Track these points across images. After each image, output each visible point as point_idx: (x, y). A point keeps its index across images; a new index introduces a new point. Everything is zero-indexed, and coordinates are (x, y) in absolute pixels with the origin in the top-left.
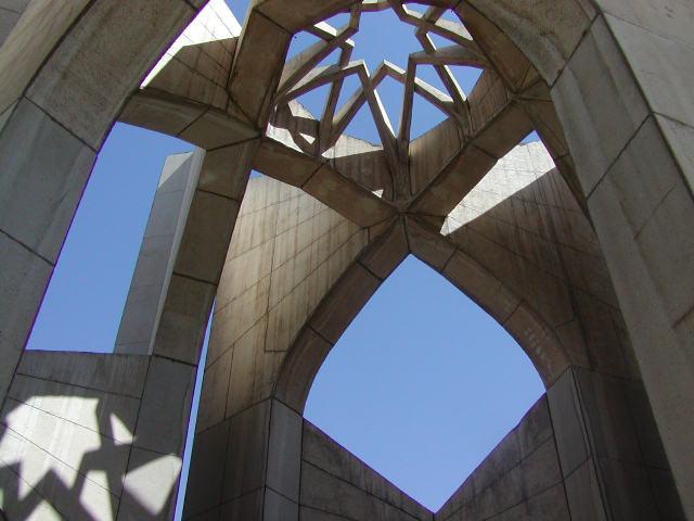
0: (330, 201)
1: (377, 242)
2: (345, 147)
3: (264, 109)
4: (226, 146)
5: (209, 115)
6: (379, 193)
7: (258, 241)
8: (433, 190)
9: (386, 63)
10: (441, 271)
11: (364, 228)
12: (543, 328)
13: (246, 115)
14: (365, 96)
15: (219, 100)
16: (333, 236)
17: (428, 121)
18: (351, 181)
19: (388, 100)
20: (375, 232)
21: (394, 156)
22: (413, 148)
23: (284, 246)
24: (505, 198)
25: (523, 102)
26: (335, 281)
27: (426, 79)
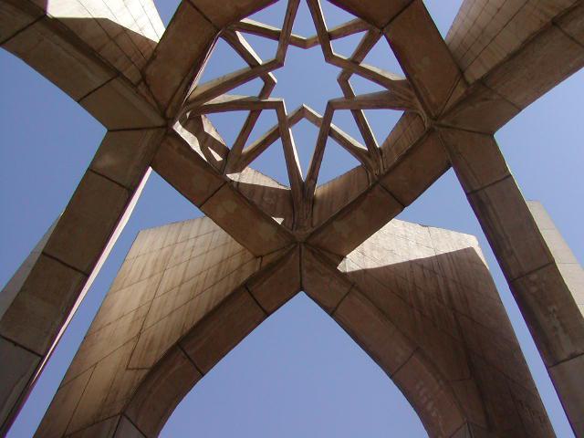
0: (225, 224)
1: (269, 270)
2: (248, 176)
3: (177, 97)
4: (128, 130)
5: (116, 83)
6: (279, 221)
7: (147, 274)
8: (336, 224)
10: (332, 312)
11: (257, 257)
12: (438, 381)
13: (157, 102)
14: (280, 133)
15: (135, 77)
16: (223, 267)
17: (337, 165)
18: (252, 203)
19: (302, 139)
20: (267, 260)
21: (300, 194)
22: (318, 191)
23: (172, 276)
24: (405, 260)
25: (441, 130)
26: (216, 304)
27: (343, 123)
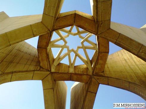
9: (81, 42)
10: (108, 84)
